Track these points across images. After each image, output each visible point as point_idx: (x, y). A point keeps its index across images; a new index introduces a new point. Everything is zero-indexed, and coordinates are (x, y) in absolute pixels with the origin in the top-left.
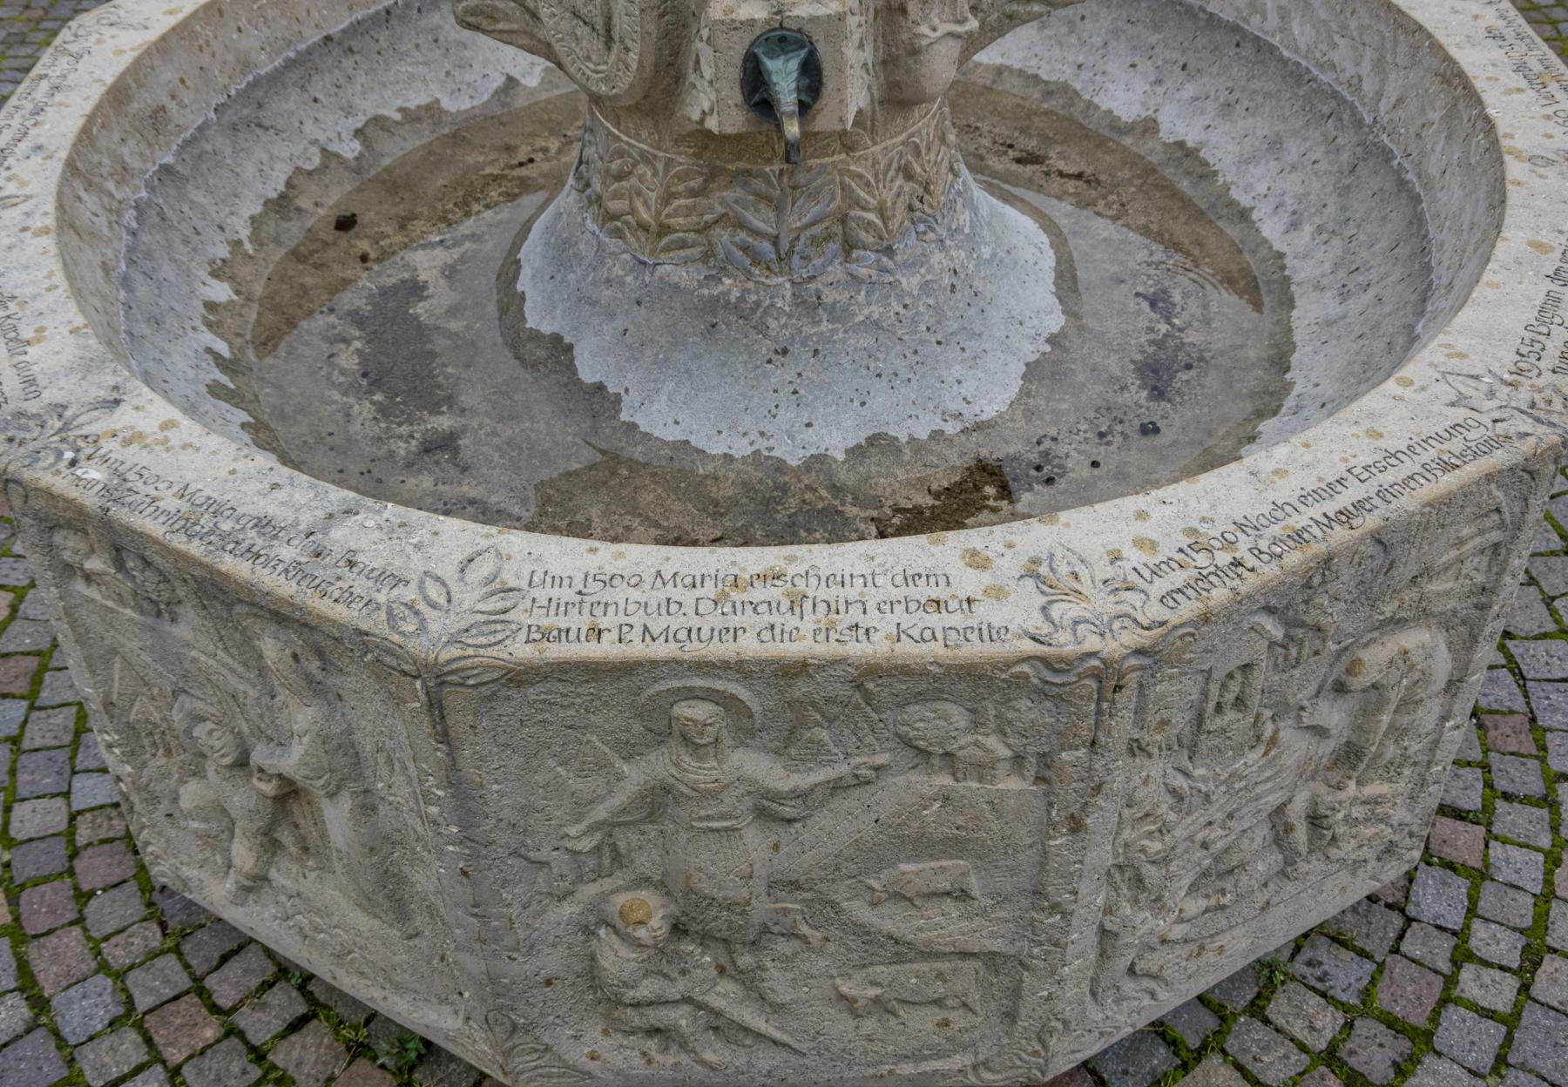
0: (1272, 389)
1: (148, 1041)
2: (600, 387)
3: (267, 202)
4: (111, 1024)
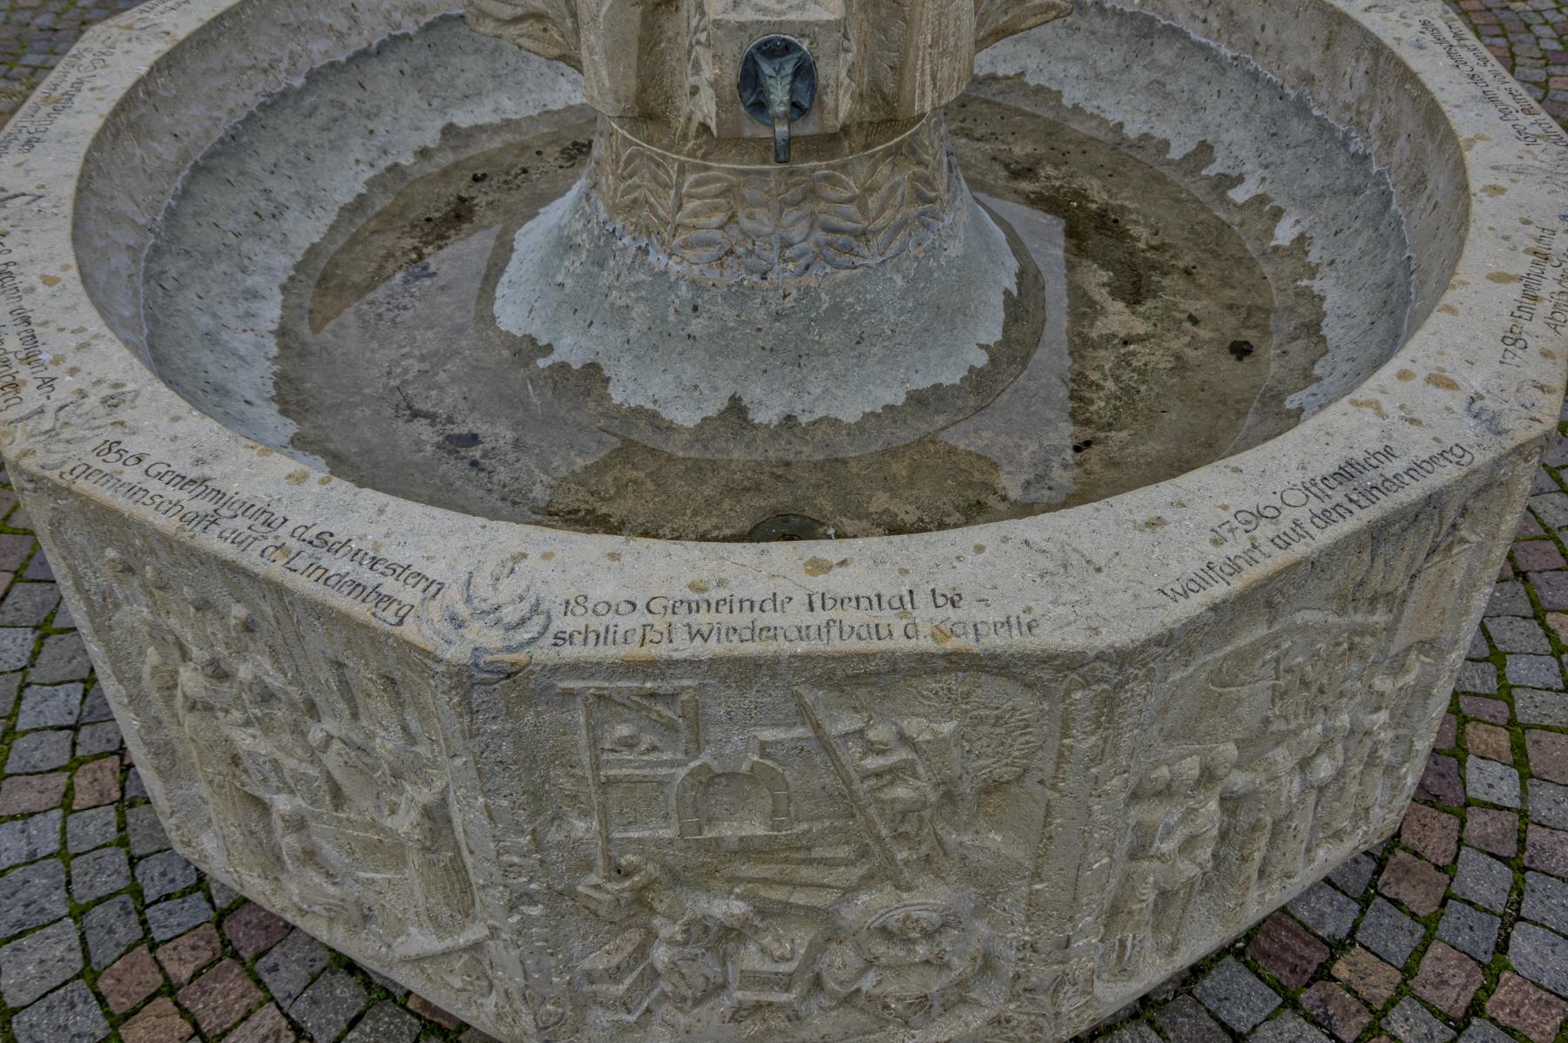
0: (381, 189)
3: (1325, 314)
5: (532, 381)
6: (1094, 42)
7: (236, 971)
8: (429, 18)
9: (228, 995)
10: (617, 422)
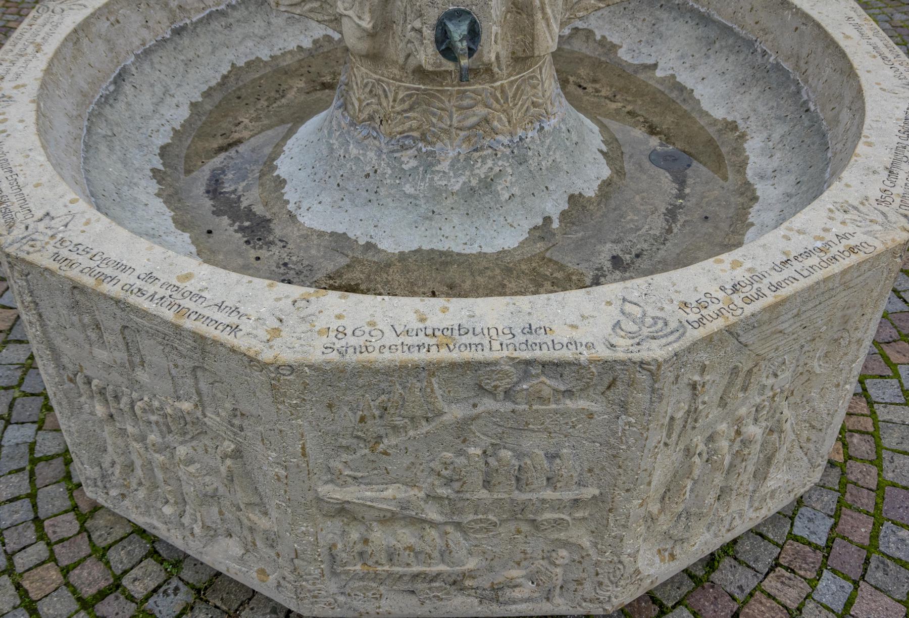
5: (565, 234)
6: (243, 25)
7: (747, 610)
9: (762, 611)
10: (603, 200)
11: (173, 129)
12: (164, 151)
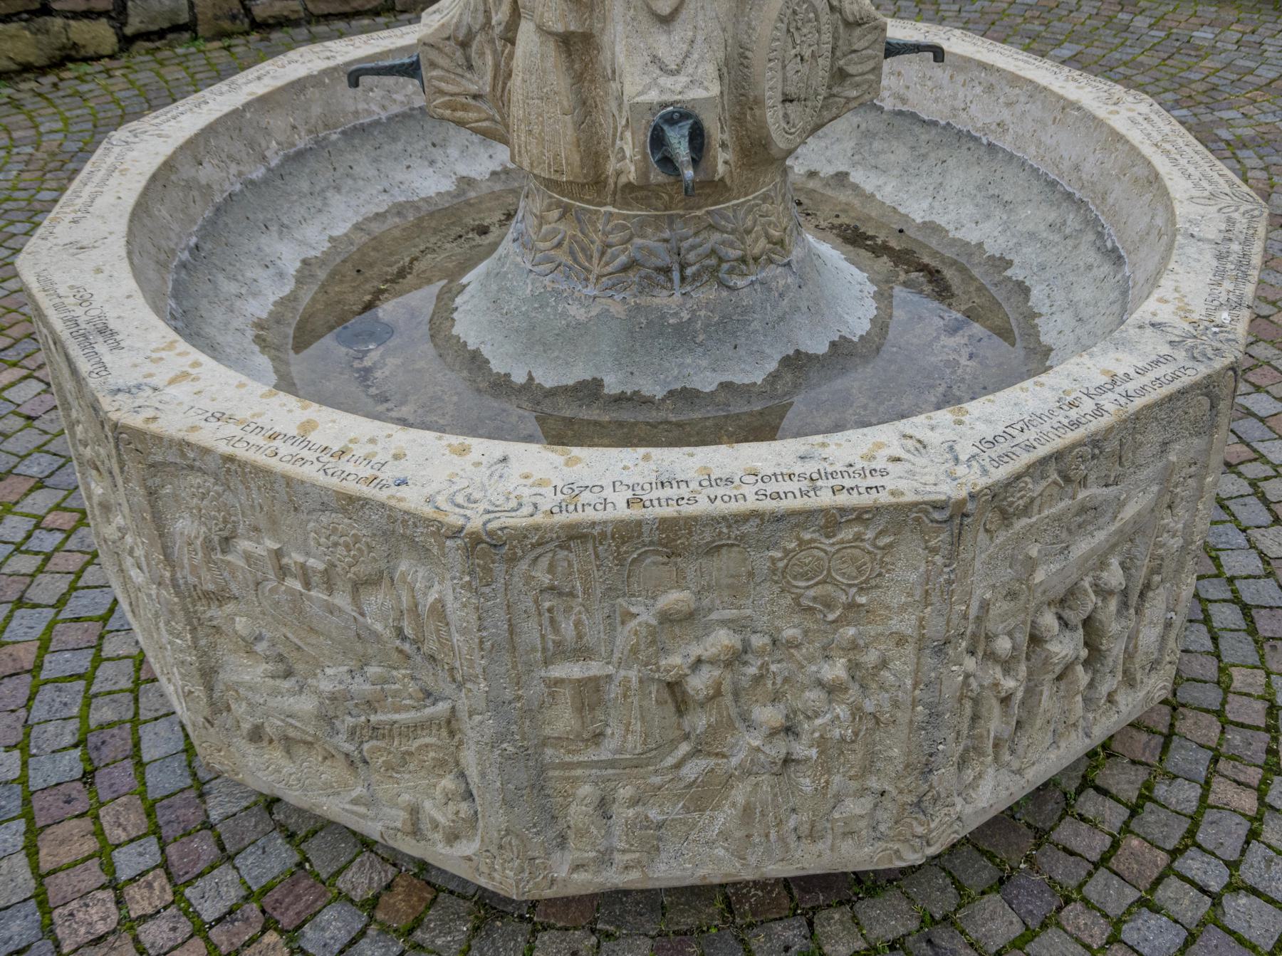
1: (1158, 881)
2: (833, 344)
4: (1158, 912)
8: (904, 108)
11: (1040, 315)
12: (1023, 290)
